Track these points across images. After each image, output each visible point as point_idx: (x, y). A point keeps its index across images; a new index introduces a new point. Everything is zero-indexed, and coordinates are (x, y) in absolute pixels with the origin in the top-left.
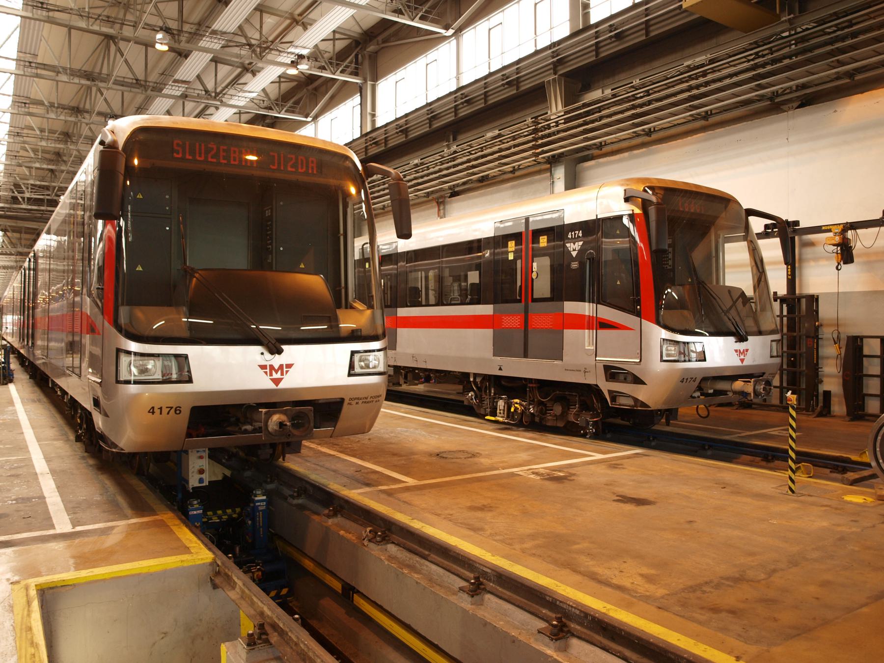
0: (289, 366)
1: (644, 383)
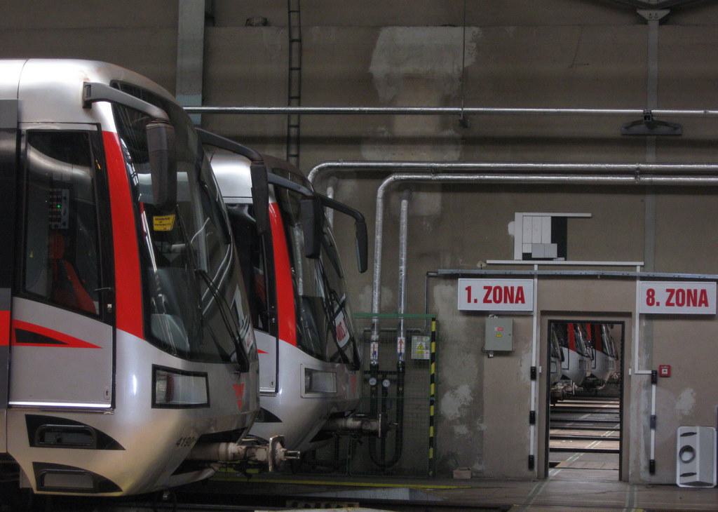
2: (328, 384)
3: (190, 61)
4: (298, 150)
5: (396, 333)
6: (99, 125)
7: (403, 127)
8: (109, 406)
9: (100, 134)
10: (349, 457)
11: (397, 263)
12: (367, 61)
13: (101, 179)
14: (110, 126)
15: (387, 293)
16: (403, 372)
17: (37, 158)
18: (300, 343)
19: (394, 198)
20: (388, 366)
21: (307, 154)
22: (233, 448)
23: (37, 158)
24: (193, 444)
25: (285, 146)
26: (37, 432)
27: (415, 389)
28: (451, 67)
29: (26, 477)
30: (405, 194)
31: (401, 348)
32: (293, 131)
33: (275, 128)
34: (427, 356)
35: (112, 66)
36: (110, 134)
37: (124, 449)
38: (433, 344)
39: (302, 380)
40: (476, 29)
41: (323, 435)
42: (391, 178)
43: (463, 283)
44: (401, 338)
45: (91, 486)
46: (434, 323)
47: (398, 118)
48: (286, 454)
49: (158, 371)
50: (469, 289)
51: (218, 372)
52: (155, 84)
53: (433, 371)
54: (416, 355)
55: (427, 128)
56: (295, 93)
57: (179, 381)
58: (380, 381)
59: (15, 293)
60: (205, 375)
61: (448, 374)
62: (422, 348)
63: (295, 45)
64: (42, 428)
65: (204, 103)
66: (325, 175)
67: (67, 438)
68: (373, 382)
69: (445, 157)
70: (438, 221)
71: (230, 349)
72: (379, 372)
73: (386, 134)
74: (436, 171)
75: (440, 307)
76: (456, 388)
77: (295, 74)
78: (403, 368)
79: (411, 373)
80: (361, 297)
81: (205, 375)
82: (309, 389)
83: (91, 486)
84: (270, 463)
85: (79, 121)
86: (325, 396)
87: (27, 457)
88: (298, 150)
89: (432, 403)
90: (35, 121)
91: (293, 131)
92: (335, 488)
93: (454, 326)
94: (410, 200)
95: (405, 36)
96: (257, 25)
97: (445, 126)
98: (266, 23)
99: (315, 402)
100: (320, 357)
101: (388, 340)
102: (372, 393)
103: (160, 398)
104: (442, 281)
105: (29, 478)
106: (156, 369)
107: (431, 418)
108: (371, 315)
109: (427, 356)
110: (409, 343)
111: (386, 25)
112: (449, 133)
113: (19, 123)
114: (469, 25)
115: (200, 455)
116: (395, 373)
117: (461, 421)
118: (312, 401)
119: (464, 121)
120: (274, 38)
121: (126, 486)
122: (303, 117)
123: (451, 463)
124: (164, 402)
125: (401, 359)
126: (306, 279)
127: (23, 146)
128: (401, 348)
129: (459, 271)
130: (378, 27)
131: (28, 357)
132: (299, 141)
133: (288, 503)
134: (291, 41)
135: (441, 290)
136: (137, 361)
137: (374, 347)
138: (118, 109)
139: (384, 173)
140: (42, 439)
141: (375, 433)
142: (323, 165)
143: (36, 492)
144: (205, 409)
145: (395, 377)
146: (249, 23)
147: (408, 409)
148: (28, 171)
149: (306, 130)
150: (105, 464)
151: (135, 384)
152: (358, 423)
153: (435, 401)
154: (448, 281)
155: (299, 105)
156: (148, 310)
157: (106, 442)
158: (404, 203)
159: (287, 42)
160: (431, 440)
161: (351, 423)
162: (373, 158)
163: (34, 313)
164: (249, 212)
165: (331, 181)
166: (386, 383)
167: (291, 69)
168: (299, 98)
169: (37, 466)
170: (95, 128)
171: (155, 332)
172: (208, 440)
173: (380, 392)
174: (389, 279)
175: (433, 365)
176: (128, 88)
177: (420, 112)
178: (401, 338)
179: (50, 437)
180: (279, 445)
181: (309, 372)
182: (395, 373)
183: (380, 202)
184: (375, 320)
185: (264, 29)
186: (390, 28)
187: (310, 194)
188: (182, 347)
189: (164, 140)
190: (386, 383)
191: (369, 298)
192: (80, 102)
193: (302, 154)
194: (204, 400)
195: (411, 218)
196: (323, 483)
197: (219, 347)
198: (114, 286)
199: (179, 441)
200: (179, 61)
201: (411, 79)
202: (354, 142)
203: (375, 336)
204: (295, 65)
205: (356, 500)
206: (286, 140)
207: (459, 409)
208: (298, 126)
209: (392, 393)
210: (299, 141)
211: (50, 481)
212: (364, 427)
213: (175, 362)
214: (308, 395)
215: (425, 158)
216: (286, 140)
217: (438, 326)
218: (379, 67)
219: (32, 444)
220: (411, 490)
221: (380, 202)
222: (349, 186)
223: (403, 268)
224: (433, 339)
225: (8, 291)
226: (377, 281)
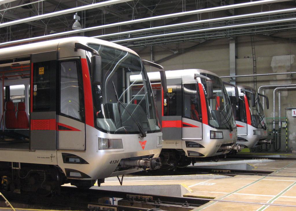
0: (146, 142)
1: (87, 163)
2: (259, 133)
3: (233, 66)
4: (256, 84)
5: (279, 122)
6: (198, 82)
7: (279, 77)
8: (201, 139)
9: (198, 84)
10: (269, 148)
11: (278, 107)
12: (270, 64)
13: (198, 93)
14: (200, 82)
15: (276, 113)
16: (280, 130)
17: (186, 90)
18: (252, 125)
19: (277, 93)
20: (277, 129)
21: (258, 84)
22: (230, 147)
23: (186, 90)
24: (220, 146)
25: (253, 83)
26: (188, 144)
27: (283, 133)
28: (288, 64)
29: (186, 154)
30: (280, 92)
31: (280, 125)
32: (255, 80)
33: (251, 79)
34: (285, 127)
35: (200, 70)
36: (200, 84)
37: (204, 147)
38: (287, 124)
39: (252, 133)
40: (294, 55)
41: (259, 144)
42: (276, 89)
43: (293, 110)
44: (280, 123)
45: (199, 155)
46: (287, 119)
47: (277, 75)
48: (241, 148)
49: (211, 132)
50: (294, 112)
51: (226, 132)
52: (212, 73)
53: (287, 130)
54: (283, 126)
55: (284, 77)
56: (255, 72)
57: (216, 133)
58: (275, 132)
59: (182, 117)
60: (222, 132)
61: (290, 130)
62: (284, 125)
63: (255, 62)
64: (189, 144)
65: (236, 75)
66: (262, 89)
67: (194, 146)
68: (274, 132)
69: (288, 83)
70: (287, 97)
71: (229, 127)
72: (275, 130)
73: (275, 79)
74: (286, 86)
75: (288, 116)
76: (292, 133)
77: (255, 67)
78: (280, 129)
79: (282, 130)
80: (271, 114)
81: (222, 132)
82: (255, 134)
83: (199, 155)
84: (237, 150)
85: (193, 81)
86: (258, 136)
87: (186, 150)
88: (256, 84)
89: (287, 136)
90: (185, 82)
91: (255, 80)
92: (265, 155)
93: (291, 119)
94: (281, 93)
95: (278, 58)
96: (246, 58)
97: (288, 76)
98: (248, 57)
99: (256, 137)
100: (257, 127)
101: (277, 123)
102: (274, 135)
103: (212, 137)
104: (289, 110)
105: (187, 154)
106: (211, 131)
107: (287, 140)
108: (273, 118)
109: (285, 127)
110: (281, 124)
111: (274, 56)
112: (289, 78)
113: (182, 83)
114: (292, 54)
115: (223, 148)
116: (278, 130)
117: (294, 140)
118: (255, 137)
119: (292, 75)
120: (250, 60)
121: (206, 155)
122: (257, 77)
123: (292, 149)
124: (214, 138)
125: (280, 127)
126: (251, 110)
127: (183, 87)
128: (280, 125)
129: (292, 108)
130: (272, 56)
131: (185, 129)
132: (256, 82)
133: (253, 158)
134: (254, 61)
135: (288, 112)
136: (207, 129)
137: (274, 125)
138: (202, 79)
139: (275, 87)
140: (189, 146)
141: (270, 143)
142: (262, 86)
143: (188, 156)
144: (222, 139)
145: (279, 131)
146: (245, 57)
147: (282, 138)
148: (184, 92)
149: (258, 79)
150: (201, 151)
151: (208, 135)
152: (266, 141)
153: (287, 136)
154: (290, 110)
155: (256, 74)
156: (209, 119)
157: (201, 146)
158: (279, 94)
159: (253, 61)
160: (287, 144)
161: (265, 141)
162: (272, 84)
163: (186, 121)
164: (240, 97)
165: (263, 90)
166: (277, 133)
167: (254, 67)
168: (256, 73)
169: (188, 151)
170: (197, 83)
171: (211, 124)
172: (224, 145)
173: (275, 134)
174: (277, 110)
175: (287, 128)
176: (204, 74)
177: (282, 74)
178: (280, 123)
179: (190, 146)
180: (239, 146)
181: (254, 131)
182: (278, 130)
183: (274, 94)
184: (274, 119)
185: (248, 58)
186: (275, 56)
187: (252, 93)
188: (217, 127)
189: (210, 84)
190: (277, 133)
191: (272, 114)
192: (194, 78)
193: (257, 84)
194: (222, 137)
195: (281, 97)
196: (263, 154)
197: (226, 126)
198: (201, 114)
199: (217, 146)
200: (230, 67)
201: (280, 67)
202: (268, 81)
203: (274, 123)
204: (255, 66)
205: (267, 158)
206: (254, 82)
207: (293, 138)
208: (256, 79)
209: (278, 134)
210: (256, 82)
211: (191, 154)
212: (268, 142)
213: (215, 130)
214: (254, 136)
215: (284, 84)
216: (254, 82)
217: (288, 120)
218: (273, 65)
219: (187, 147)
220: (280, 155)
221: (274, 94)
222: (268, 91)
223: (280, 108)
224: (286, 123)
225: (181, 116)
226: (274, 111)
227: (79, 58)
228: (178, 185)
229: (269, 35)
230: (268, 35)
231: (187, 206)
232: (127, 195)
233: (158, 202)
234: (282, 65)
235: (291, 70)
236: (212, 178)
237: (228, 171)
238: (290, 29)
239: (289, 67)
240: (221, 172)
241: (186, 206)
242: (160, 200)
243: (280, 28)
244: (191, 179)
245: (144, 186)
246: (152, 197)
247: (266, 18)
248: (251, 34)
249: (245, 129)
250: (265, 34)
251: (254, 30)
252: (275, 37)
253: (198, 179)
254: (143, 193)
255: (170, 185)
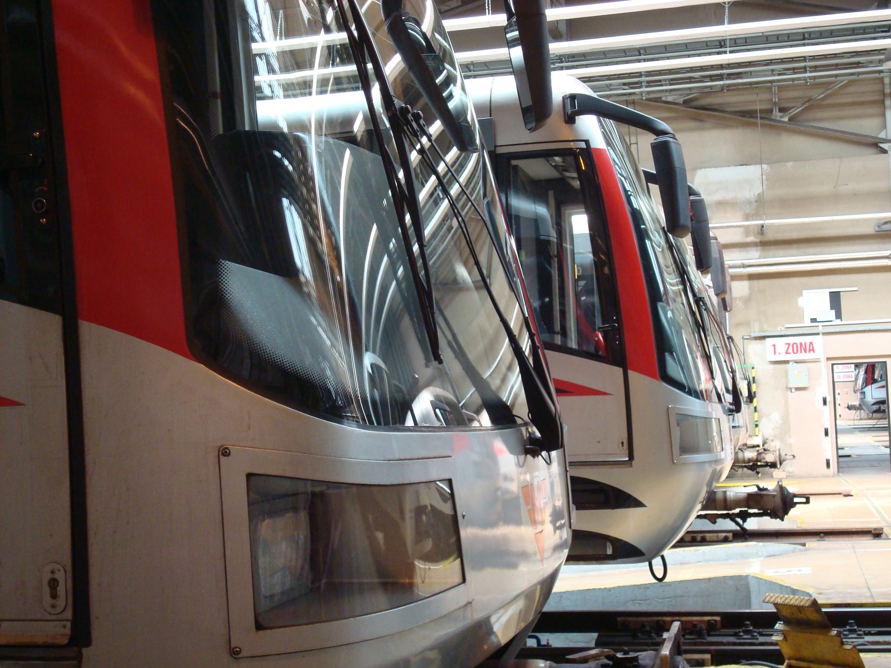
74: (744, 266)
97: (747, 234)
104: (754, 342)
111: (700, 168)
112: (751, 239)
227: (583, 145)
228: (740, 578)
229: (681, 101)
230: (677, 101)
231: (859, 635)
232: (619, 619)
233: (748, 632)
234: (729, 196)
235: (756, 215)
236: (757, 555)
237: (724, 534)
238: (757, 83)
239: (750, 203)
240: (699, 539)
241: (854, 636)
242: (752, 625)
243: (727, 79)
244: (681, 564)
245: (609, 590)
246: (718, 618)
247: (666, 50)
248: (632, 98)
249: (615, 405)
250: (670, 99)
251: (639, 85)
252: (704, 108)
253: (707, 561)
254: (665, 609)
255: (710, 579)
